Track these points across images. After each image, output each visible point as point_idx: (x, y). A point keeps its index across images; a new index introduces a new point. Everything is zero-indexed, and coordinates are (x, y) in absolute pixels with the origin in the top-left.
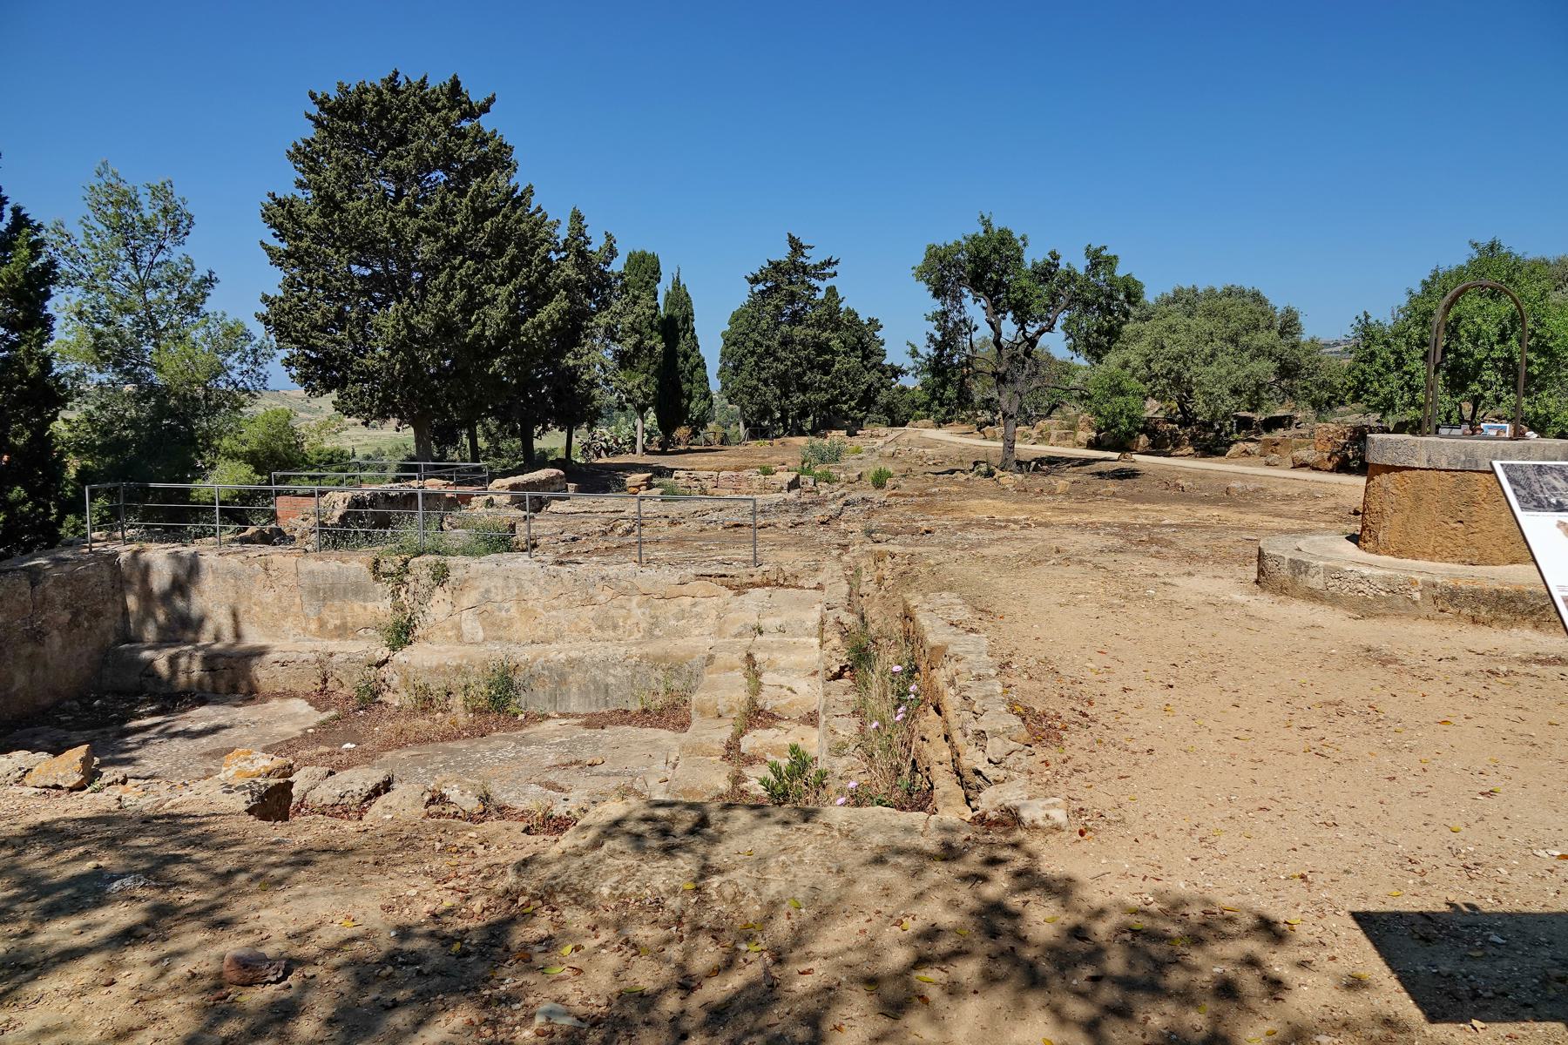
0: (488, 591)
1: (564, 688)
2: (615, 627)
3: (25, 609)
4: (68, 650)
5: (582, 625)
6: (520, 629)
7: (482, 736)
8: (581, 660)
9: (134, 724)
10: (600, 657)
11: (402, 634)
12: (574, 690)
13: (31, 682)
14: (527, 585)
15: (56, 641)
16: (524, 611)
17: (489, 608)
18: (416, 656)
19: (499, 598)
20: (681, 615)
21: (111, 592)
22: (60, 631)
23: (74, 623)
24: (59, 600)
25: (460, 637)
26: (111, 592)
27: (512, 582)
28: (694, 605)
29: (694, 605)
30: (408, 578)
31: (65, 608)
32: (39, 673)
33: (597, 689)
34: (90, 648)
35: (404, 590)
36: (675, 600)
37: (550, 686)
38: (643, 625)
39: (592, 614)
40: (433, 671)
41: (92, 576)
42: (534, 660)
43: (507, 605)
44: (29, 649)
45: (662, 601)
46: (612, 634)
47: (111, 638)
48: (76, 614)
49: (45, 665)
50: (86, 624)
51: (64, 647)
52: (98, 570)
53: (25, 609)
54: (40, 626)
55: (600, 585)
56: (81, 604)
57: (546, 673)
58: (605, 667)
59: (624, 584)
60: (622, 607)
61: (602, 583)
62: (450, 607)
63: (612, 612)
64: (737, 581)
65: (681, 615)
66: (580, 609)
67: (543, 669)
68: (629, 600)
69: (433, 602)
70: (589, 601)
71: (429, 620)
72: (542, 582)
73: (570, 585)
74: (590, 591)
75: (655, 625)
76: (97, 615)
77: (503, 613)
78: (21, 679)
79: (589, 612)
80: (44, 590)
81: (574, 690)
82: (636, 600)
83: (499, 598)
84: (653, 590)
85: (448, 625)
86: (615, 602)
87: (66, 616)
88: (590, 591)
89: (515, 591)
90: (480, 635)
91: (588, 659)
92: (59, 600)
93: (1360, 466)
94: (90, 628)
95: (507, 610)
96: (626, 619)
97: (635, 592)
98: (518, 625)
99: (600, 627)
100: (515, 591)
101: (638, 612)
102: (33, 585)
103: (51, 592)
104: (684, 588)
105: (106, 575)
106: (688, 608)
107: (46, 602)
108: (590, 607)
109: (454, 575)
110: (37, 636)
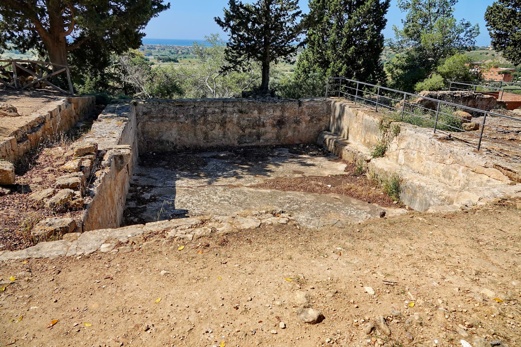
0: (409, 143)
1: (415, 198)
2: (450, 178)
3: (295, 113)
4: (307, 129)
5: (437, 172)
6: (416, 165)
7: (369, 203)
8: (423, 188)
9: (300, 156)
10: (430, 190)
11: (381, 152)
12: (418, 200)
13: (293, 136)
14: (423, 145)
15: (303, 125)
16: (419, 157)
17: (408, 151)
18: (379, 163)
19: (412, 148)
20: (481, 184)
21: (326, 114)
22: (306, 122)
23: (311, 121)
24: (307, 113)
25: (397, 160)
26: (326, 114)
27: (418, 143)
28: (488, 181)
29: (488, 181)
30: (388, 130)
31: (309, 116)
32: (296, 133)
33: (426, 204)
34: (315, 130)
35: (386, 134)
36: (480, 175)
37: (411, 194)
38: (462, 182)
39: (442, 168)
40: (380, 170)
41: (319, 107)
42: (408, 180)
43: (414, 152)
44: (294, 125)
45: (473, 173)
46: (448, 181)
47: (323, 128)
48: (312, 118)
49: (299, 131)
50: (315, 122)
51: (306, 127)
52: (322, 105)
53: (295, 113)
54: (299, 119)
55: (449, 155)
56: (314, 115)
57: (411, 187)
58: (431, 195)
59: (459, 158)
60: (455, 169)
61: (450, 154)
62: (397, 146)
63: (451, 171)
64: (516, 176)
65: (481, 184)
66: (438, 164)
67: (410, 185)
68: (459, 167)
69: (393, 142)
70: (443, 161)
71: (391, 149)
72: (428, 146)
73: (437, 150)
74: (445, 156)
75: (467, 184)
76: (320, 120)
77: (412, 155)
78: (290, 134)
79: (441, 167)
80: (302, 109)
81: (418, 200)
82: (462, 168)
83: (412, 148)
84: (471, 166)
85: (395, 154)
86: (453, 166)
87: (309, 118)
88: (445, 156)
89: (418, 147)
90: (403, 163)
91: (426, 189)
92: (307, 113)
93: (158, 8)
94: (316, 123)
95: (414, 155)
96: (456, 176)
97: (463, 164)
98: (415, 162)
99: (444, 176)
100: (418, 147)
101: (461, 175)
102: (300, 106)
103: (304, 110)
104: (486, 170)
105: (325, 108)
106: (485, 182)
107: (302, 113)
108: (442, 164)
109: (402, 132)
110: (297, 122)
